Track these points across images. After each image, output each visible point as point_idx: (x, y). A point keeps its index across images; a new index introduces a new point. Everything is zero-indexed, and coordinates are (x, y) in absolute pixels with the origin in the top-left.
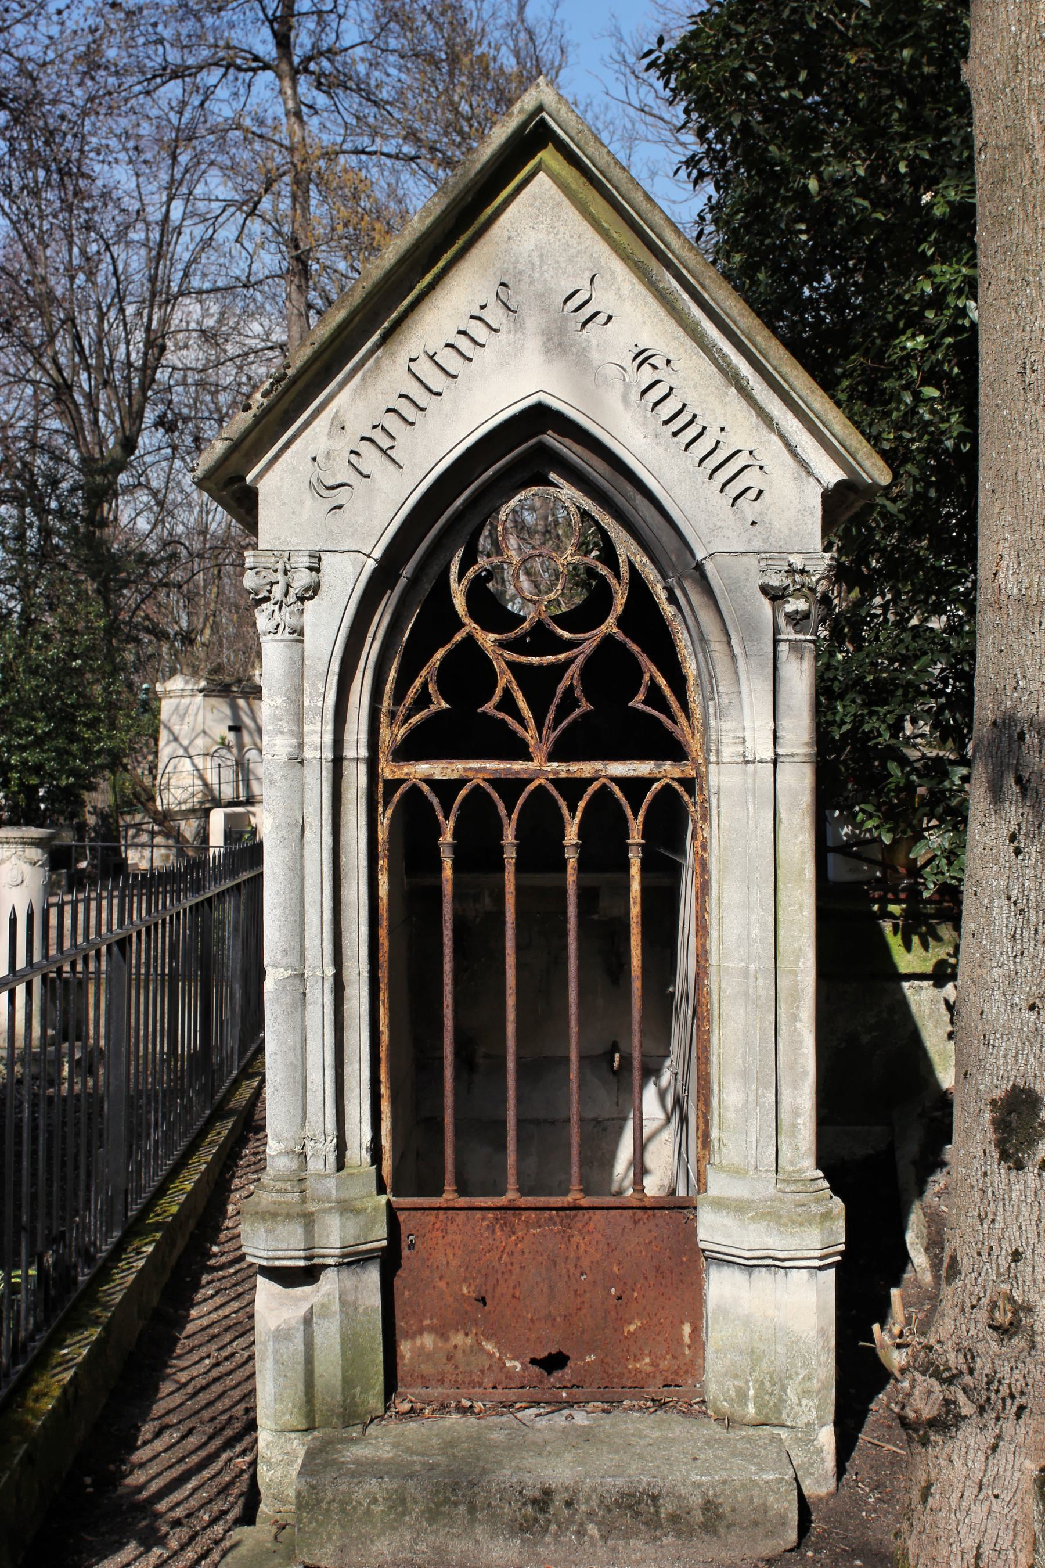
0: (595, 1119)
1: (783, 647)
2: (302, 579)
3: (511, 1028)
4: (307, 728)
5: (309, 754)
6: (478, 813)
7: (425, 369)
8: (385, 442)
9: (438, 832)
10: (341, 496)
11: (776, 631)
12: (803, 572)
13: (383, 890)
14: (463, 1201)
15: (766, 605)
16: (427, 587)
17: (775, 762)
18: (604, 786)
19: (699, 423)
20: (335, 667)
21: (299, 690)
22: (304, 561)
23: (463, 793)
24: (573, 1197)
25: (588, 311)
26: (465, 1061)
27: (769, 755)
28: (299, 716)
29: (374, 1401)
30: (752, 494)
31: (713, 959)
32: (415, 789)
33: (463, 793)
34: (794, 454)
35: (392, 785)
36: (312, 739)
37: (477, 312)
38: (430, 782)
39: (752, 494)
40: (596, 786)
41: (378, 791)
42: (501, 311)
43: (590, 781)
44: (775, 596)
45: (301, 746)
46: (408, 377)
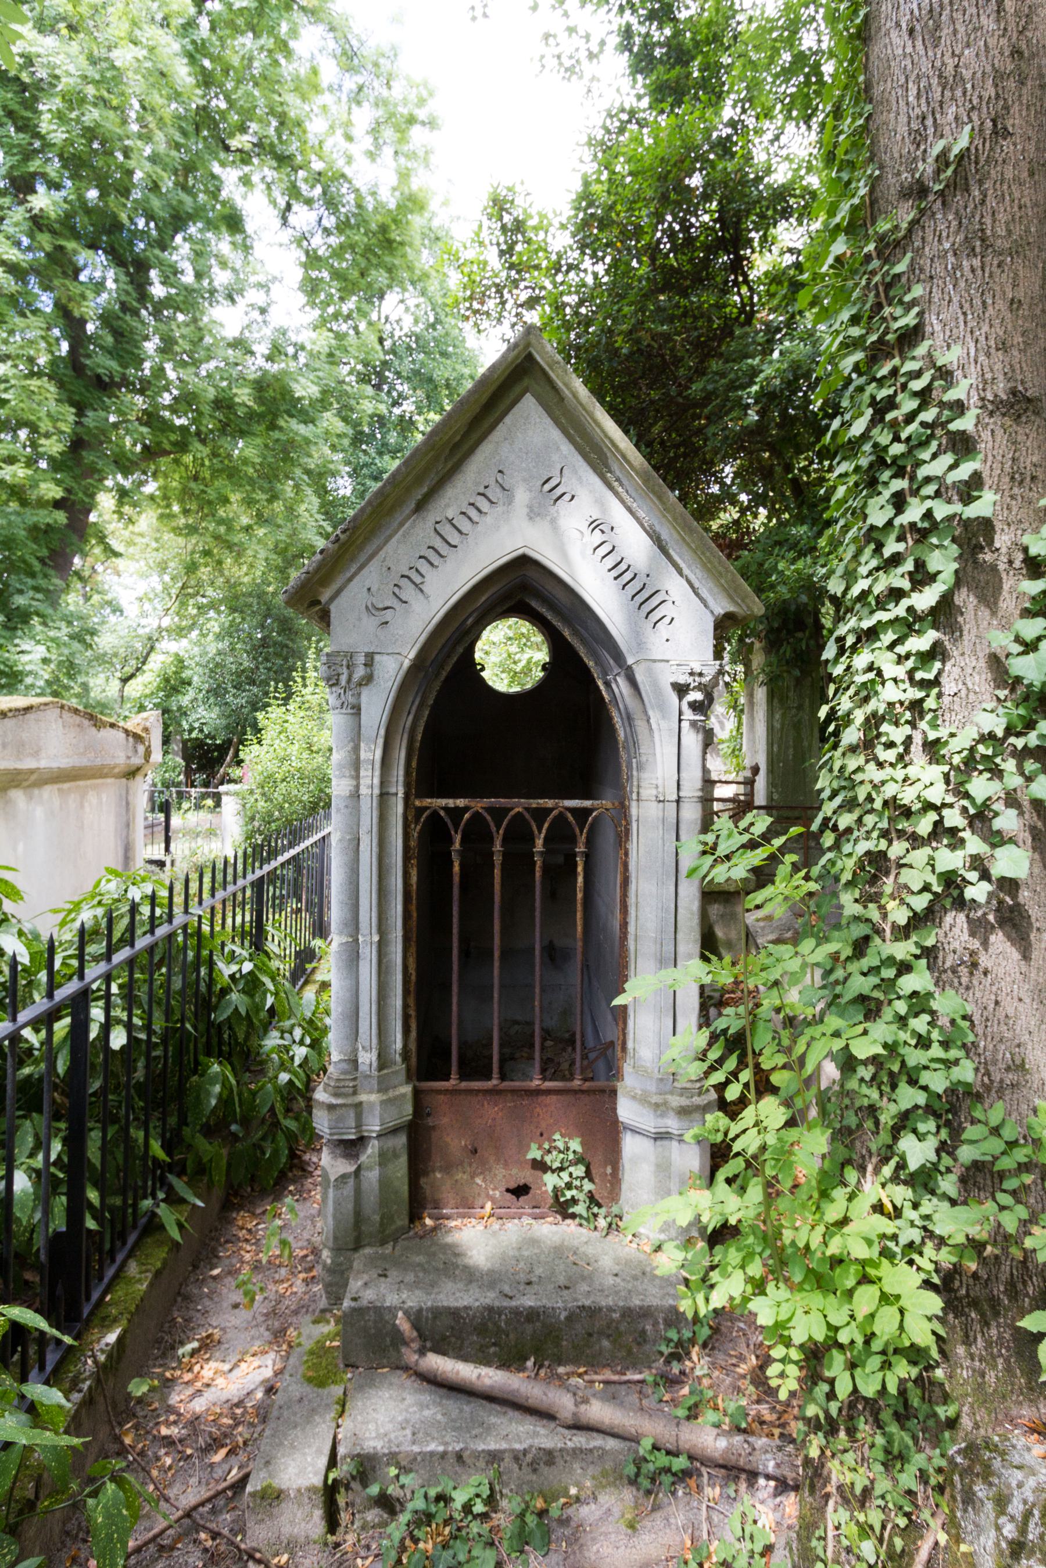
0: (567, 1216)
1: (685, 725)
2: (360, 672)
3: (497, 887)
4: (362, 773)
5: (364, 791)
6: (477, 833)
7: (447, 530)
8: (418, 579)
9: (450, 841)
10: (388, 615)
11: (680, 713)
12: (701, 675)
13: (414, 879)
14: (464, 1085)
15: (674, 697)
16: (460, 650)
17: (678, 801)
18: (561, 814)
19: (615, 573)
20: (382, 732)
21: (356, 749)
22: (361, 659)
23: (467, 816)
24: (536, 1083)
25: (558, 491)
26: (465, 954)
27: (675, 797)
28: (356, 765)
29: (402, 1221)
30: (667, 620)
31: (631, 929)
32: (435, 814)
33: (467, 816)
34: (697, 594)
35: (421, 810)
36: (365, 782)
37: (482, 490)
38: (446, 809)
39: (667, 620)
40: (555, 813)
41: (412, 815)
42: (498, 490)
43: (551, 810)
44: (681, 690)
45: (357, 787)
46: (433, 534)
